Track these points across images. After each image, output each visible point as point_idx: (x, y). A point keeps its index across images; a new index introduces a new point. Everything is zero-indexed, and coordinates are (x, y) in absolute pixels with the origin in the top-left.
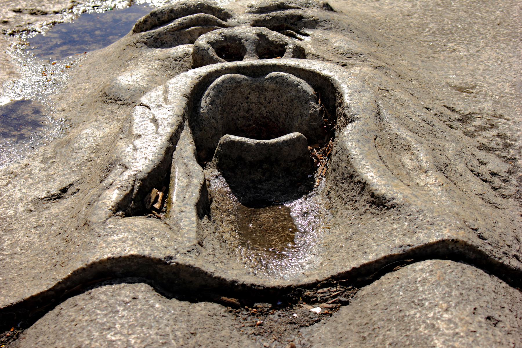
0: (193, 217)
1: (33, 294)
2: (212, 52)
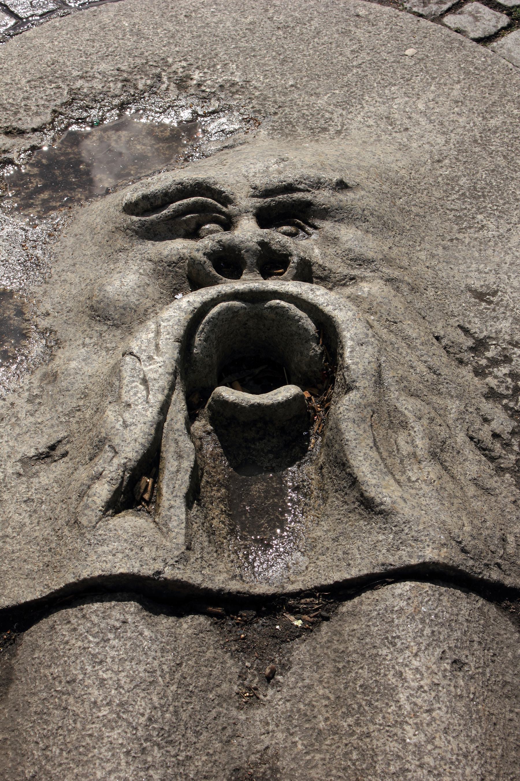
0: (182, 514)
1: (28, 600)
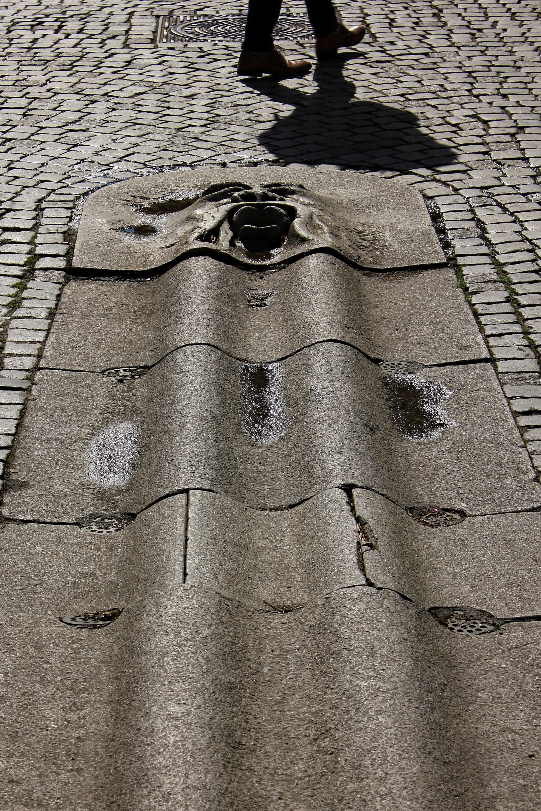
2: (240, 198)
